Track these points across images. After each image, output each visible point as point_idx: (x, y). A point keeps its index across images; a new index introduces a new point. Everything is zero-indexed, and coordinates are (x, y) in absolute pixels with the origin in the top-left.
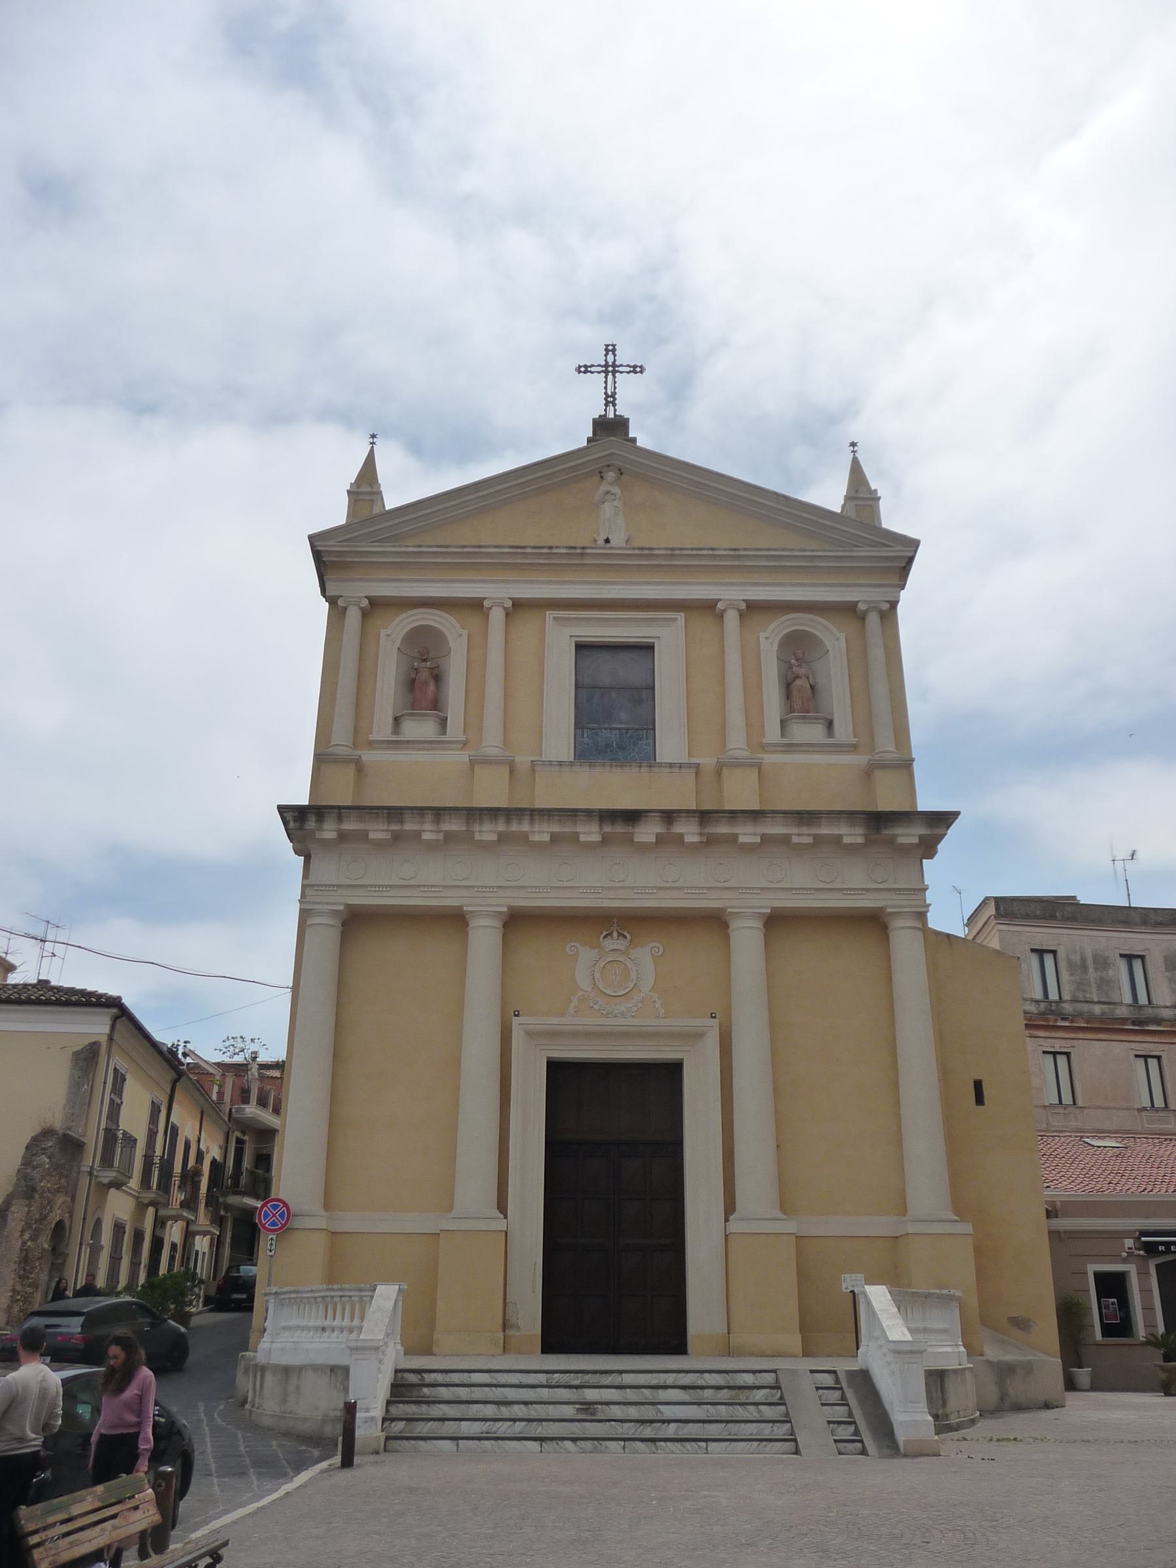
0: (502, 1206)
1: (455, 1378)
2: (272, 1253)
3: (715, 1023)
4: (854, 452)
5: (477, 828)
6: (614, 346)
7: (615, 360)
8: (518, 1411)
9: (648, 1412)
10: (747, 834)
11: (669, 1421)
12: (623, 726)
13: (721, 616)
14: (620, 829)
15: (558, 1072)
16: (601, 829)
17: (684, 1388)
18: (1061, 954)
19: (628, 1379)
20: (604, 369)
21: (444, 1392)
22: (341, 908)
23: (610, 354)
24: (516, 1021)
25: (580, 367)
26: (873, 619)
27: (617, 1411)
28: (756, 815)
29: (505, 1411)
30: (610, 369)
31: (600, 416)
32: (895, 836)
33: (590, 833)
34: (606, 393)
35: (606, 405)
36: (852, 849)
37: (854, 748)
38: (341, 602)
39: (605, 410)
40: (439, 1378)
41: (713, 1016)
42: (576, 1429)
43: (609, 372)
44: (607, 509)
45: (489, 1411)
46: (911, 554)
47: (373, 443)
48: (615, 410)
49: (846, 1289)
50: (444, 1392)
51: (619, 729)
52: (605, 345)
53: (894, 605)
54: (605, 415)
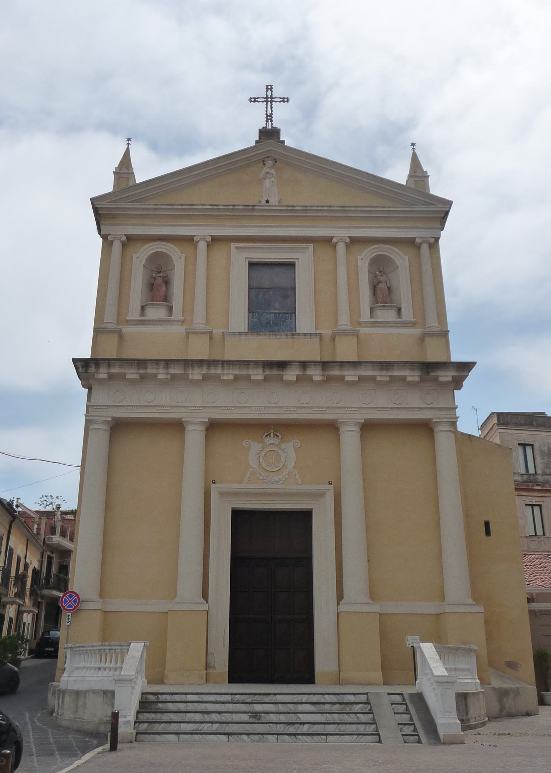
0: (205, 596)
1: (177, 698)
2: (69, 624)
3: (331, 487)
4: (413, 149)
5: (190, 372)
6: (271, 86)
7: (272, 95)
8: (215, 717)
9: (292, 718)
10: (350, 375)
11: (304, 723)
12: (277, 311)
13: (335, 246)
14: (275, 372)
15: (237, 514)
16: (264, 372)
17: (313, 703)
18: (536, 447)
19: (280, 698)
20: (265, 100)
21: (171, 707)
22: (110, 419)
23: (269, 91)
24: (213, 486)
25: (251, 98)
26: (425, 248)
27: (273, 718)
28: (355, 364)
29: (207, 718)
30: (269, 100)
31: (263, 128)
32: (438, 376)
33: (257, 375)
34: (267, 114)
35: (267, 121)
36: (412, 384)
37: (413, 324)
38: (109, 238)
39: (266, 124)
40: (168, 697)
41: (330, 483)
42: (249, 728)
43: (269, 101)
44: (267, 183)
45: (197, 717)
46: (447, 209)
47: (129, 144)
48: (272, 124)
49: (409, 645)
50: (171, 707)
51: (274, 313)
52: (266, 85)
53: (437, 239)
54: (266, 127)
